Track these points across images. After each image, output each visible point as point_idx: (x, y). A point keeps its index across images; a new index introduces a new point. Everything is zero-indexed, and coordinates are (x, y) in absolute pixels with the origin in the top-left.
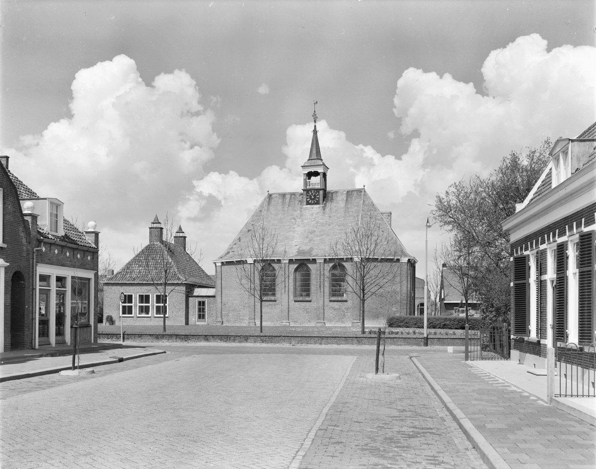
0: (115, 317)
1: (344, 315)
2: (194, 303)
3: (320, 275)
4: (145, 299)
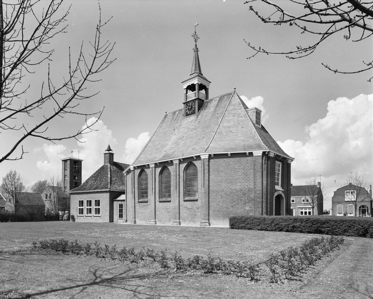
0: (75, 217)
1: (195, 215)
2: (116, 205)
3: (153, 178)
4: (89, 203)
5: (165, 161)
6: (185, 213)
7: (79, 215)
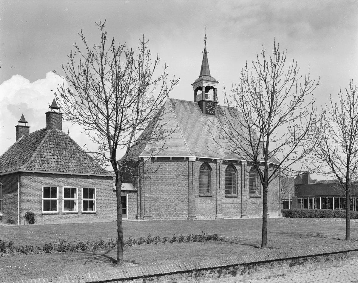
4: (69, 192)
5: (232, 160)
6: (251, 207)
7: (43, 212)
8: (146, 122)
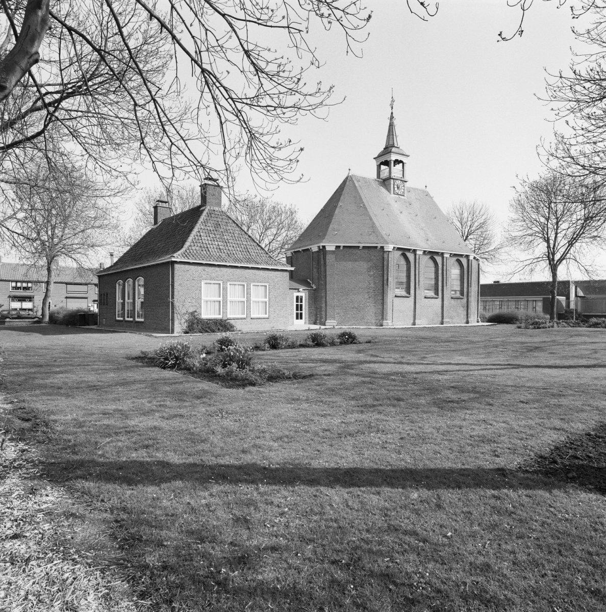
8: (483, 426)
